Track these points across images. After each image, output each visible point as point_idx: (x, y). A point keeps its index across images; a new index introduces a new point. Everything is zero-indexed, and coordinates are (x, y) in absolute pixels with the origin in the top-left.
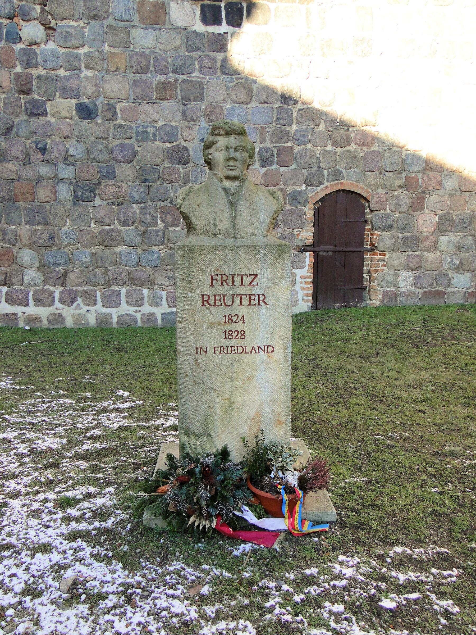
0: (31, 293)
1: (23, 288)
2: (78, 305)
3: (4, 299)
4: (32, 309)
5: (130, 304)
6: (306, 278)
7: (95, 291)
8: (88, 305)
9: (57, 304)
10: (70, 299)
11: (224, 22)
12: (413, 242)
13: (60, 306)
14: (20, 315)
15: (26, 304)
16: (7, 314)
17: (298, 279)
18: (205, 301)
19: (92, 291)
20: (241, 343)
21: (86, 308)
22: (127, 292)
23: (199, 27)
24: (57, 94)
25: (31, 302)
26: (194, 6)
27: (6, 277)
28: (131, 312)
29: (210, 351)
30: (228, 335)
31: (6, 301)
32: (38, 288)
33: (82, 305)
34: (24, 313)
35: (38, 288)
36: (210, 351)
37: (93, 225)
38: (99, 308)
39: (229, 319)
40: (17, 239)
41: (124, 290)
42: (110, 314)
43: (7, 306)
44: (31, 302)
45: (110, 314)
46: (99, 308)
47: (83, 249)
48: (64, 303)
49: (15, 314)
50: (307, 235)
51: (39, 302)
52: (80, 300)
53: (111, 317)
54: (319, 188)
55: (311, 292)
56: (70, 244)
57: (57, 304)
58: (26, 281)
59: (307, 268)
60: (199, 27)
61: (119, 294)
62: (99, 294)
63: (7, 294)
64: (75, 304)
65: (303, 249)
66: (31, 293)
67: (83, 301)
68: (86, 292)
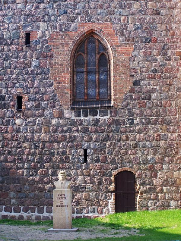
0: (13, 208)
1: (10, 206)
2: (29, 212)
3: (3, 210)
4: (13, 214)
5: (47, 212)
6: (112, 203)
7: (35, 207)
8: (32, 212)
9: (22, 212)
10: (25, 210)
11: (82, 116)
12: (152, 190)
13: (23, 212)
14: (8, 216)
15: (11, 212)
16: (4, 215)
17: (109, 204)
18: (57, 198)
19: (34, 207)
20: (63, 205)
21: (31, 214)
22: (46, 208)
23: (73, 118)
24: (26, 140)
25: (13, 211)
26: (72, 111)
27: (5, 202)
28: (48, 215)
29: (58, 206)
30: (61, 204)
31: (4, 211)
32: (15, 206)
33: (30, 212)
34: (10, 215)
35: (15, 206)
36: (58, 206)
37: (35, 184)
38: (36, 214)
39: (61, 201)
40: (9, 189)
41: (45, 207)
42: (40, 216)
43: (5, 212)
44: (13, 211)
45: (40, 216)
46: (36, 214)
47: (32, 193)
48: (24, 212)
49: (7, 215)
50: (112, 187)
51: (15, 211)
52: (29, 211)
53: (40, 217)
54: (116, 170)
55: (114, 208)
56: (27, 191)
57: (22, 212)
58: (11, 204)
59: (112, 199)
60: (73, 118)
61: (43, 209)
62: (36, 208)
63: (5, 208)
64: (28, 212)
65: (112, 192)
66: (13, 208)
67: (31, 211)
68: (32, 208)
